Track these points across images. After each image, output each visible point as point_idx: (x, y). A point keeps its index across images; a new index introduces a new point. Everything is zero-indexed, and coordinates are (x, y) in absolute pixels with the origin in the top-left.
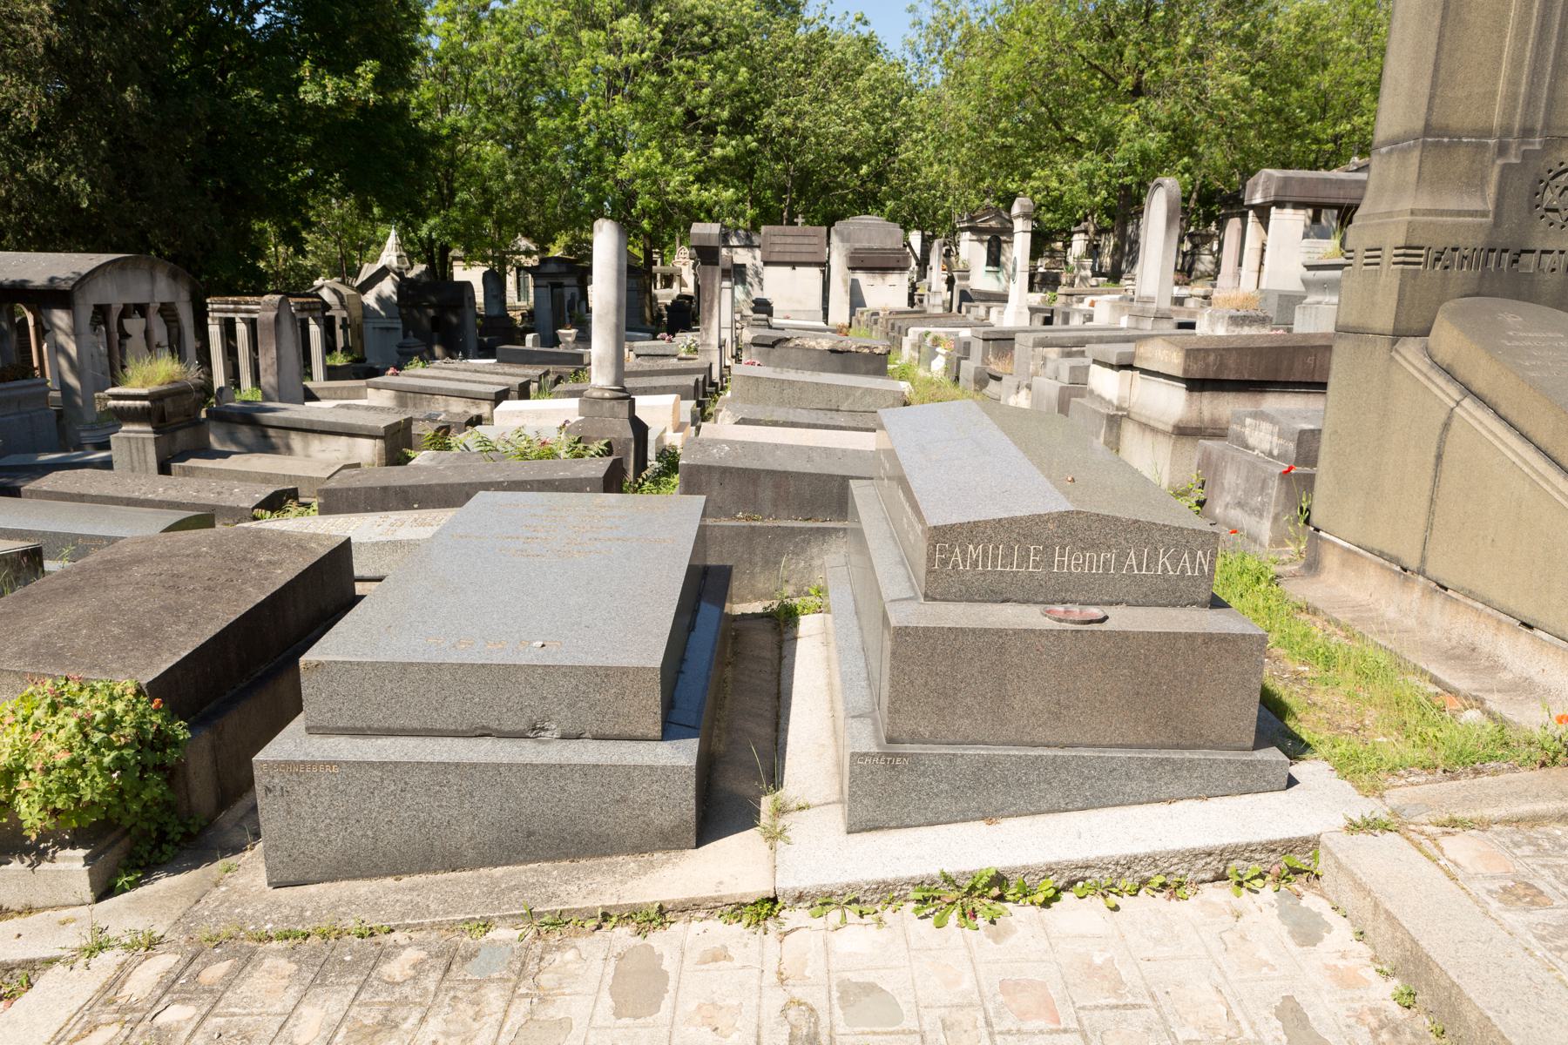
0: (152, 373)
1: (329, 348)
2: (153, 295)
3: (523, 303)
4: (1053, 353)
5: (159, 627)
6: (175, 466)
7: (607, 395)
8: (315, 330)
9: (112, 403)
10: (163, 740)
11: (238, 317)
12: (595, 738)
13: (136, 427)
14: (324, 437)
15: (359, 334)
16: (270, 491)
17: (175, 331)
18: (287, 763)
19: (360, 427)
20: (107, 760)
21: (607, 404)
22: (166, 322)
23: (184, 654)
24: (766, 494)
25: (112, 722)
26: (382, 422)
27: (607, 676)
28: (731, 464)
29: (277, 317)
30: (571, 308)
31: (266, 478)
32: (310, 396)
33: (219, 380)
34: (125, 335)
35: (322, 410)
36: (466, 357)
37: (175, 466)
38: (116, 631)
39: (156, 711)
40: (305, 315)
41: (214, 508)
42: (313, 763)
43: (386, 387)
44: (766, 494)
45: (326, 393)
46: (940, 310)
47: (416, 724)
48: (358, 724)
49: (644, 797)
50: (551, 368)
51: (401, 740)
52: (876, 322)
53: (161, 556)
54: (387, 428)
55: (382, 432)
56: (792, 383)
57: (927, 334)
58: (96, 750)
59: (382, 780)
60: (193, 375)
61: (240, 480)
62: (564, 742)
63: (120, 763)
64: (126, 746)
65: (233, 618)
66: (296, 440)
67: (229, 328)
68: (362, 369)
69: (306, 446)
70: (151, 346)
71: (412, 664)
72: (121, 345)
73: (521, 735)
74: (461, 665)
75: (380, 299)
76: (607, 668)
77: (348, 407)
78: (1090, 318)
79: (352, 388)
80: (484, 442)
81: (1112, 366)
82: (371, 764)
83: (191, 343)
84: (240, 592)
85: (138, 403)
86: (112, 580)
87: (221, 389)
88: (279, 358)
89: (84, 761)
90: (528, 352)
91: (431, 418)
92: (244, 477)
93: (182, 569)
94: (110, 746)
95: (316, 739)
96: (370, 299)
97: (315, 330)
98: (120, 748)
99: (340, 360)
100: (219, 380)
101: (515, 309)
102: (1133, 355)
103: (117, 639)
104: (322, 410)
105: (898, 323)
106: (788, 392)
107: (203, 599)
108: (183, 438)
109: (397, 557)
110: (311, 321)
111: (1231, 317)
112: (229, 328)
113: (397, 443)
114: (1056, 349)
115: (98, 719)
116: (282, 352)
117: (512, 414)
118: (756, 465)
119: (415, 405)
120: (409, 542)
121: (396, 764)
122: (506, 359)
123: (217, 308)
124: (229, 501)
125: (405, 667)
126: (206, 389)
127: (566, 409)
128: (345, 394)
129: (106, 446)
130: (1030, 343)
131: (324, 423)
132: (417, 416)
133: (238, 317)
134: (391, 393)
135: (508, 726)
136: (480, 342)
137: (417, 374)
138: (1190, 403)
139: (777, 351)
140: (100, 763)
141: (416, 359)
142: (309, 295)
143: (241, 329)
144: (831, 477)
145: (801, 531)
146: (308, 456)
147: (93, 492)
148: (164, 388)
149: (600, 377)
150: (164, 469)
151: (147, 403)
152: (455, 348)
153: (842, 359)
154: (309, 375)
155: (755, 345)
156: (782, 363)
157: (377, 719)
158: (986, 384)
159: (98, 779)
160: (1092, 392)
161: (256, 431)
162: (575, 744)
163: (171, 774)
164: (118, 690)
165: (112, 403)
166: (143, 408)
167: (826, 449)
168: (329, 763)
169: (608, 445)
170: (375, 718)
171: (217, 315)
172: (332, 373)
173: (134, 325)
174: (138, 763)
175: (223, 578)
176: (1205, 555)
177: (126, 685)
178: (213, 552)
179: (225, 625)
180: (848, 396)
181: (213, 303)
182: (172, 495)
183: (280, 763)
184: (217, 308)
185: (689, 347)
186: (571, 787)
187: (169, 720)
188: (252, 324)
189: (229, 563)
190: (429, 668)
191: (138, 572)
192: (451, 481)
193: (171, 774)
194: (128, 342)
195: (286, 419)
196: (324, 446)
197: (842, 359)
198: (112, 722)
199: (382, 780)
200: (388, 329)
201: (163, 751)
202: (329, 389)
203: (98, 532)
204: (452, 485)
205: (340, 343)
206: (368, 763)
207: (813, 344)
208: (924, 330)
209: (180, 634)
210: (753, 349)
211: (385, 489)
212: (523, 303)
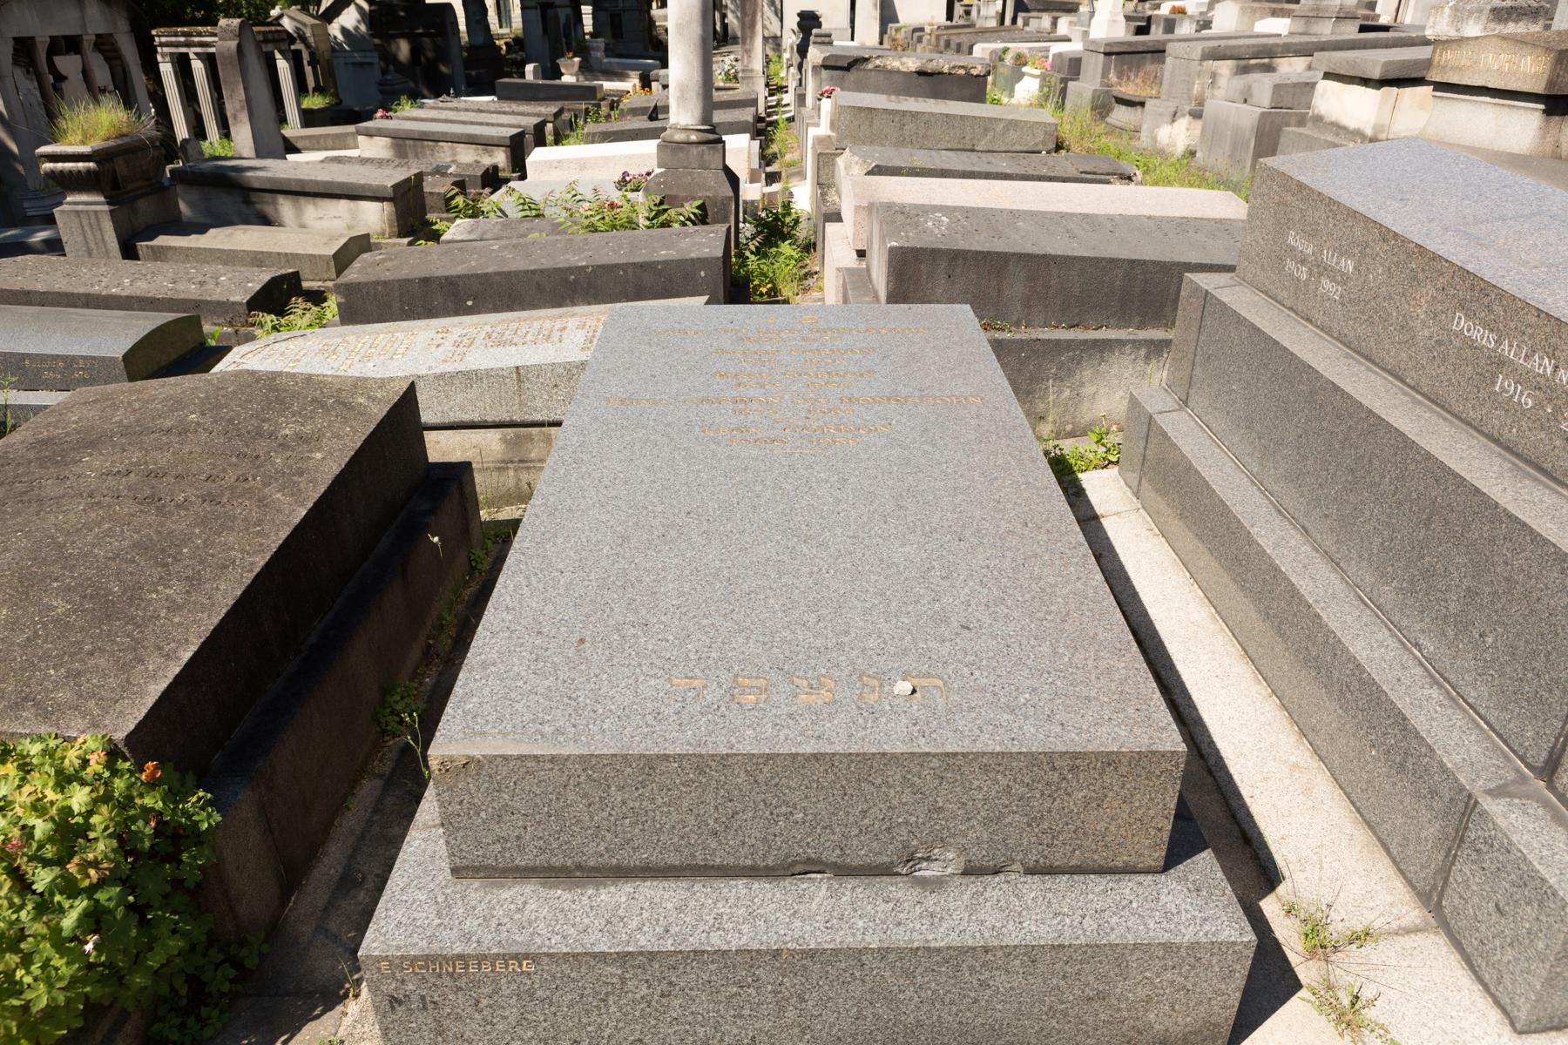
0: (92, 126)
1: (301, 88)
2: (84, 26)
3: (505, 31)
4: (1225, 67)
5: (134, 593)
6: (142, 246)
7: (693, 138)
8: (283, 65)
9: (48, 166)
10: (174, 836)
11: (192, 51)
12: (1030, 871)
13: (84, 198)
14: (320, 201)
15: (330, 73)
16: (266, 277)
17: (119, 70)
18: (429, 959)
19: (362, 186)
20: (68, 922)
21: (695, 150)
22: (107, 59)
23: (187, 655)
24: (1016, 288)
25: (69, 833)
26: (390, 177)
27: (1074, 769)
28: (962, 244)
29: (239, 46)
30: (567, 36)
31: (257, 259)
32: (290, 147)
33: (182, 131)
34: (60, 78)
35: (306, 164)
36: (457, 95)
37: (142, 246)
38: (61, 606)
39: (152, 785)
40: (268, 48)
41: (197, 304)
42: (481, 958)
43: (380, 133)
44: (1016, 288)
45: (308, 144)
46: (993, 23)
47: (674, 859)
48: (557, 861)
49: (1142, 992)
50: (566, 104)
51: (649, 890)
52: (920, 40)
53: (126, 431)
54: (396, 187)
55: (390, 193)
56: (915, 115)
57: (1005, 50)
58: (44, 906)
59: (623, 981)
60: (147, 126)
61: (225, 263)
62: (975, 885)
63: (94, 920)
64: (102, 883)
65: (260, 561)
66: (285, 207)
67: (182, 65)
68: (345, 114)
69: (299, 213)
70: (95, 93)
71: (666, 758)
72: (57, 89)
73: (886, 871)
74: (769, 757)
75: (344, 30)
76: (1076, 755)
77: (338, 160)
78: (1207, 24)
79: (337, 136)
80: (526, 203)
81: (1365, 82)
82: (603, 957)
83: (139, 80)
84: (262, 502)
85: (81, 165)
86: (51, 488)
87: (185, 141)
88: (248, 100)
89: (22, 935)
90: (530, 86)
91: (440, 171)
92: (230, 258)
93: (164, 458)
94: (70, 888)
95: (474, 890)
96: (334, 29)
97: (283, 65)
98: (91, 891)
99: (315, 102)
100: (182, 131)
101: (500, 37)
102: (1428, 64)
103: (62, 624)
104: (306, 164)
105: (955, 40)
106: (910, 126)
107: (203, 522)
108: (146, 208)
109: (472, 394)
110: (278, 55)
111: (1494, 10)
112: (182, 65)
113: (413, 212)
114: (1230, 63)
115: (38, 834)
116: (252, 93)
117: (550, 165)
118: (999, 246)
119: (416, 156)
120: (488, 373)
121: (652, 956)
122: (509, 95)
123: (165, 40)
124: (217, 295)
125: (650, 764)
126: (167, 146)
127: (642, 155)
128: (330, 143)
129: (50, 221)
130: (1197, 54)
131: (317, 182)
132: (423, 168)
133: (192, 51)
134: (385, 141)
135: (860, 854)
136: (468, 77)
137: (413, 116)
138: (1544, 130)
139: (853, 76)
140: (56, 930)
141: (403, 99)
142: (270, 24)
143: (198, 66)
144: (1113, 262)
145: (1070, 345)
146: (303, 226)
147: (41, 287)
148: (111, 143)
149: (683, 115)
150: (129, 252)
151: (91, 165)
152: (439, 87)
153: (930, 82)
154: (283, 120)
155: (825, 67)
156: (860, 87)
157: (594, 852)
158: (1110, 110)
159: (58, 962)
160: (1318, 119)
161: (239, 199)
162: (995, 888)
163: (196, 896)
164: (72, 758)
165: (48, 166)
166: (89, 171)
167: (1085, 216)
168: (516, 957)
169: (702, 207)
170: (591, 848)
171: (166, 50)
172: (309, 118)
173: (68, 64)
174: (131, 908)
175: (231, 476)
176: (1511, 346)
177: (87, 746)
178: (207, 421)
179: (248, 578)
180: (986, 130)
181: (160, 36)
182: (142, 288)
183: (415, 958)
184: (165, 40)
185: (727, 74)
186: (1001, 980)
187: (175, 795)
188: (210, 61)
189: (237, 442)
190: (701, 764)
191: (91, 466)
192: (513, 267)
193: (196, 896)
194: (65, 86)
195: (269, 179)
196: (321, 212)
197: (930, 82)
198: (69, 833)
199: (623, 981)
200: (361, 64)
201: (175, 859)
202: (310, 137)
203: (48, 351)
204: (517, 274)
205: (311, 83)
206: (594, 956)
207: (896, 64)
208: (1000, 46)
209: (174, 608)
210: (824, 73)
211: (426, 281)
212: (505, 31)
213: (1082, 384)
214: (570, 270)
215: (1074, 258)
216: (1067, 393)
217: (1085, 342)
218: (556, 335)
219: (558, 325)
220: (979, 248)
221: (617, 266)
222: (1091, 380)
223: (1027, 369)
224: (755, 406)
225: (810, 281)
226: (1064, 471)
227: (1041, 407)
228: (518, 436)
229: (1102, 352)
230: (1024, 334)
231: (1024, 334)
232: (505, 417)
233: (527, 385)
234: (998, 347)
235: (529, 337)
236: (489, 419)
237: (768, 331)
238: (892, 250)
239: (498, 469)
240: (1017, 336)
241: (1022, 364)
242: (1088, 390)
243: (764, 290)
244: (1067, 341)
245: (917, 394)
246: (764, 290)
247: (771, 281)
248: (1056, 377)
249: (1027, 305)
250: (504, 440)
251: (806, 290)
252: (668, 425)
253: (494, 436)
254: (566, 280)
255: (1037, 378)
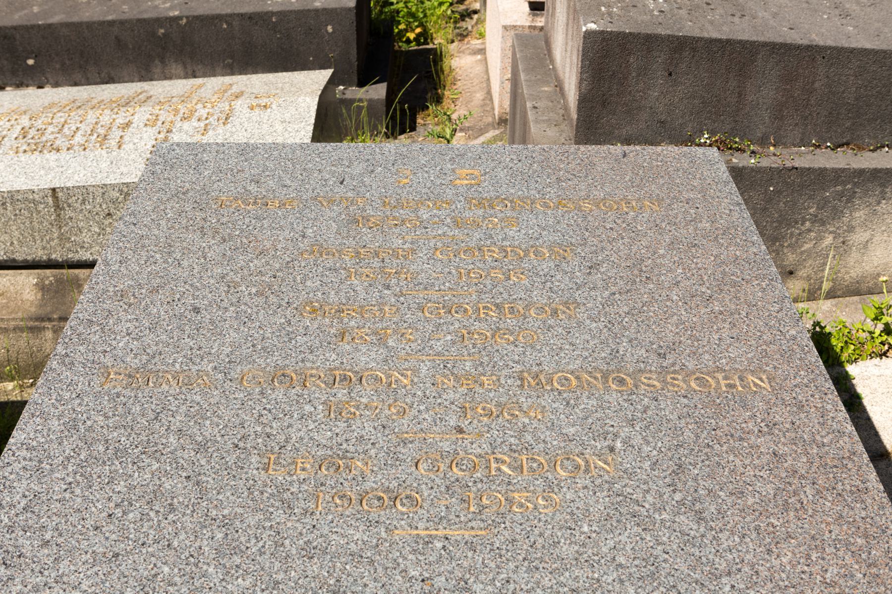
24: (764, 92)
28: (690, 28)
44: (764, 92)
118: (742, 31)
145: (838, 176)
213: (851, 229)
214: (159, 21)
215: (852, 51)
216: (829, 240)
217: (861, 172)
218: (116, 134)
219: (120, 120)
220: (715, 35)
221: (219, 17)
222: (864, 225)
223: (780, 205)
224: (366, 394)
225: (468, 24)
226: (832, 361)
227: (791, 258)
228: (59, 281)
229: (883, 186)
230: (773, 158)
231: (773, 158)
232: (40, 255)
233: (69, 213)
234: (737, 173)
235: (79, 139)
236: (19, 257)
237: (399, 205)
238: (589, 34)
239: (31, 329)
240: (765, 163)
241: (770, 201)
242: (859, 236)
243: (412, 36)
244: (835, 171)
245: (654, 363)
246: (412, 36)
247: (421, 25)
248: (815, 219)
249: (778, 113)
250: (41, 287)
251: (463, 36)
252: (201, 447)
253: (27, 280)
254: (154, 34)
255: (785, 221)
